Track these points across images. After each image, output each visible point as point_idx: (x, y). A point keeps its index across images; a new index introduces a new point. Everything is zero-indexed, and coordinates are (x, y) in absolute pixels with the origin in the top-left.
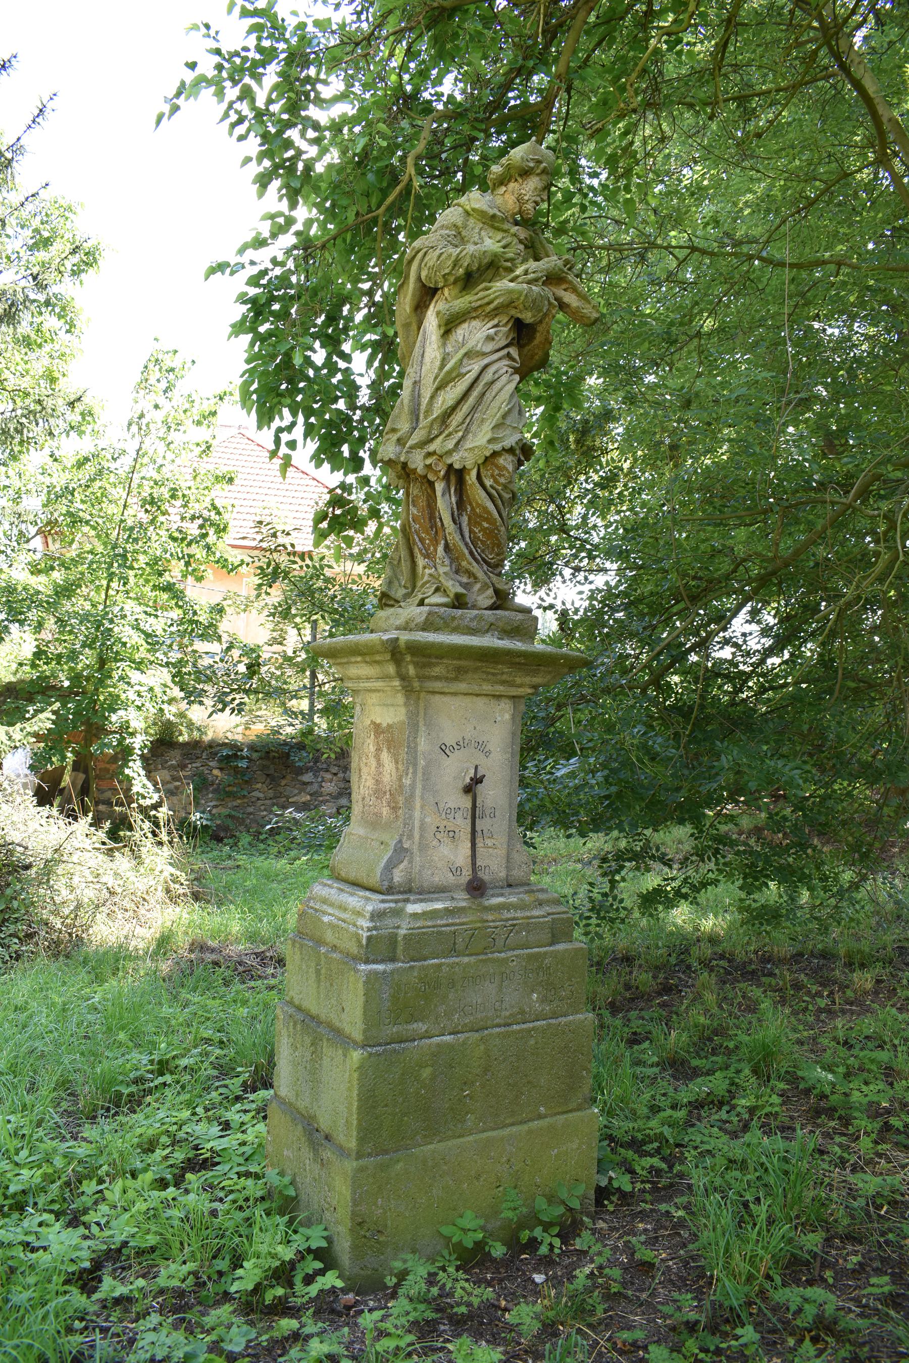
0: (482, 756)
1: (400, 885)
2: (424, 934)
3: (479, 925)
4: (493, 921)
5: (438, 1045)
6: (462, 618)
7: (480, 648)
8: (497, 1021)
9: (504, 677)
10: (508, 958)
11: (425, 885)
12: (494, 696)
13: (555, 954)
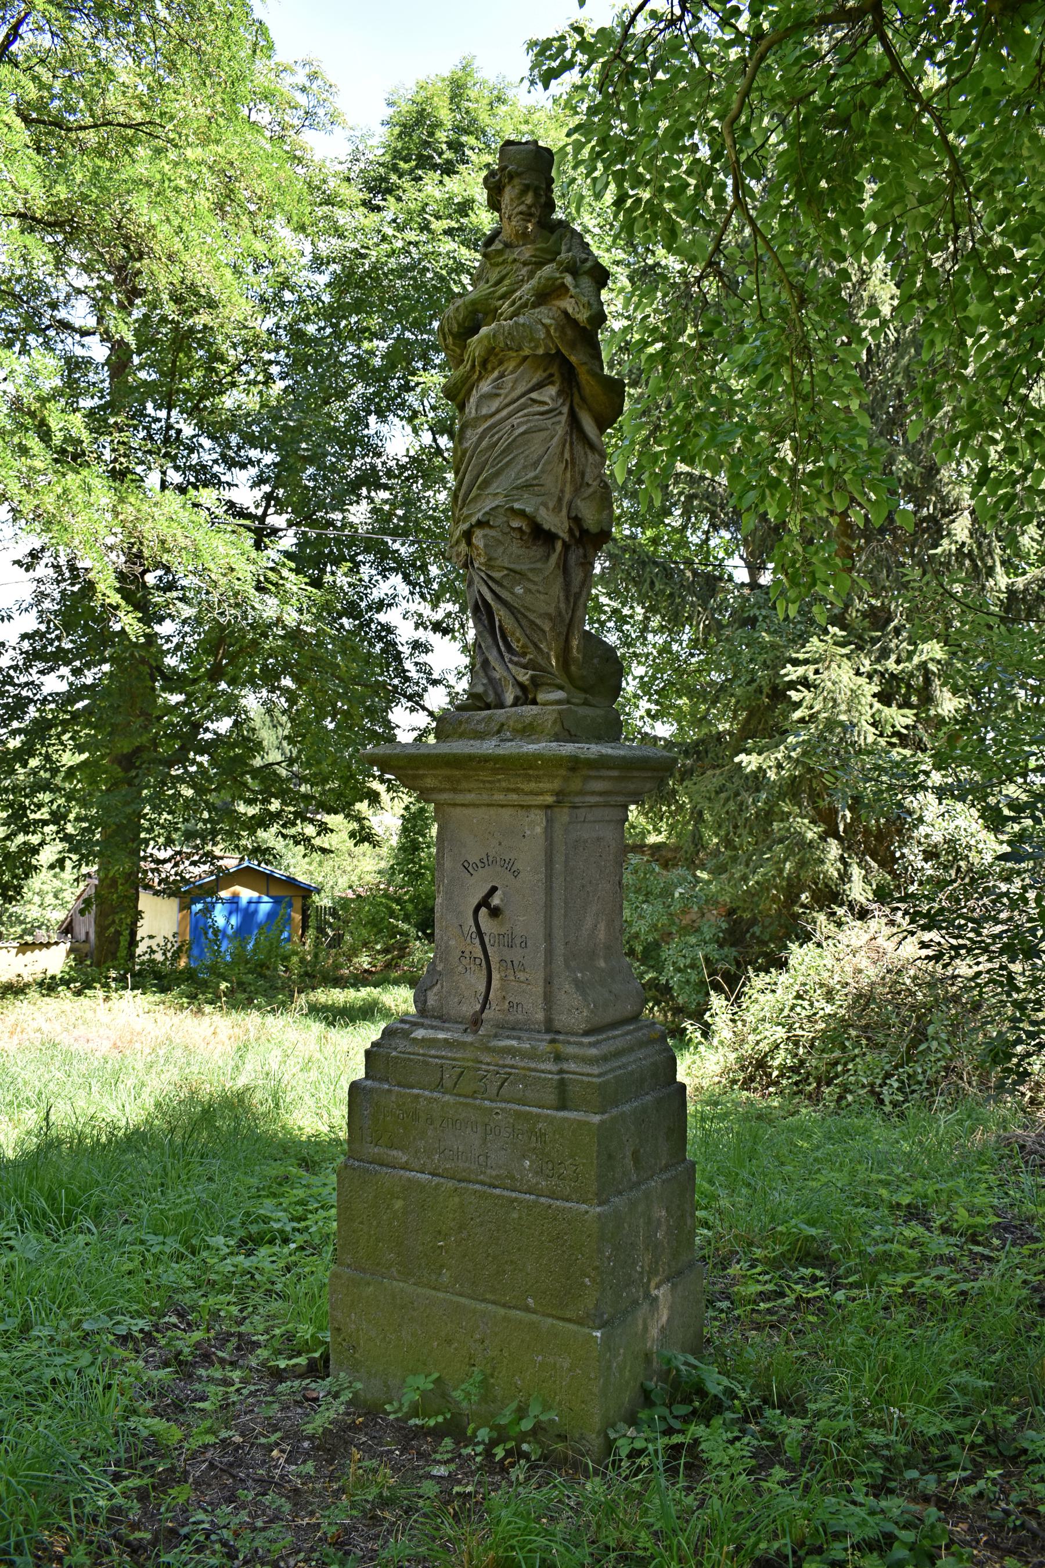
0: (510, 876)
1: (433, 1009)
2: (411, 1060)
3: (470, 1064)
4: (488, 1064)
5: (409, 1180)
6: (468, 721)
7: (624, 757)
8: (481, 1177)
9: (504, 784)
10: (492, 1109)
11: (452, 1012)
12: (522, 806)
13: (550, 1120)
